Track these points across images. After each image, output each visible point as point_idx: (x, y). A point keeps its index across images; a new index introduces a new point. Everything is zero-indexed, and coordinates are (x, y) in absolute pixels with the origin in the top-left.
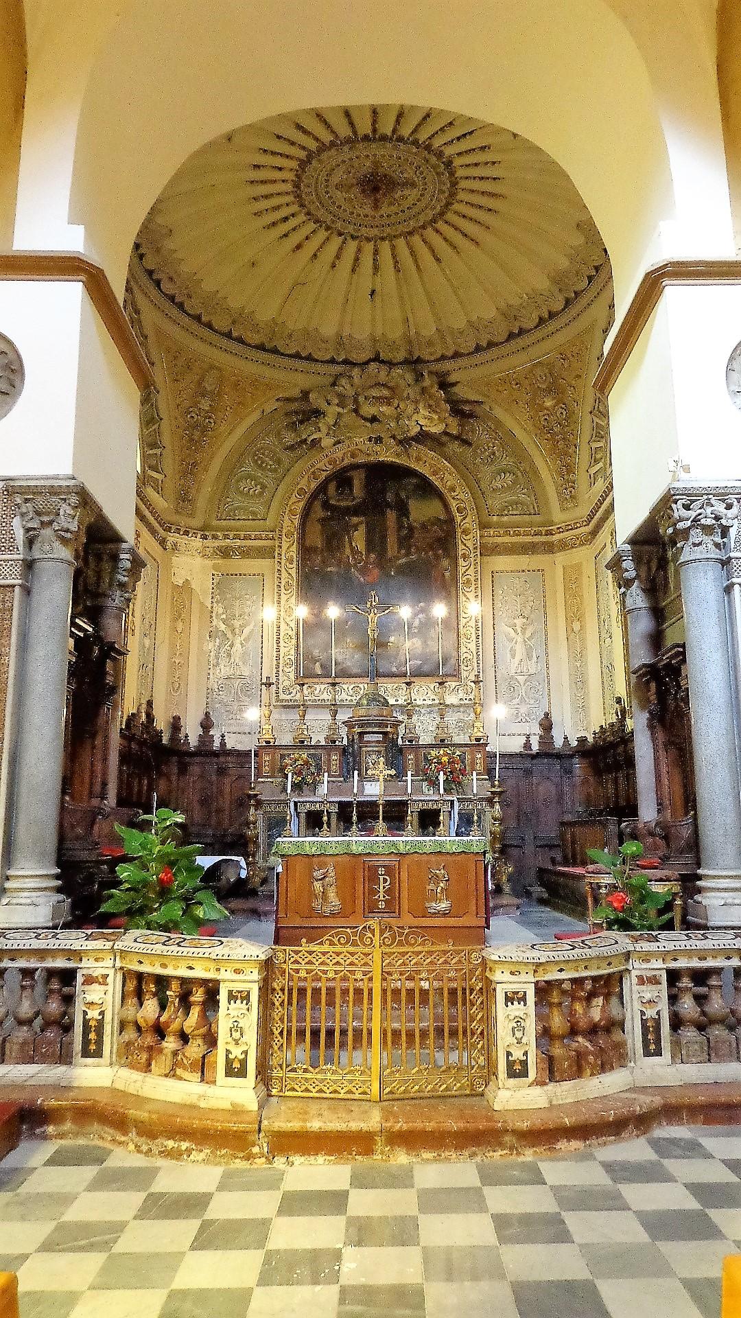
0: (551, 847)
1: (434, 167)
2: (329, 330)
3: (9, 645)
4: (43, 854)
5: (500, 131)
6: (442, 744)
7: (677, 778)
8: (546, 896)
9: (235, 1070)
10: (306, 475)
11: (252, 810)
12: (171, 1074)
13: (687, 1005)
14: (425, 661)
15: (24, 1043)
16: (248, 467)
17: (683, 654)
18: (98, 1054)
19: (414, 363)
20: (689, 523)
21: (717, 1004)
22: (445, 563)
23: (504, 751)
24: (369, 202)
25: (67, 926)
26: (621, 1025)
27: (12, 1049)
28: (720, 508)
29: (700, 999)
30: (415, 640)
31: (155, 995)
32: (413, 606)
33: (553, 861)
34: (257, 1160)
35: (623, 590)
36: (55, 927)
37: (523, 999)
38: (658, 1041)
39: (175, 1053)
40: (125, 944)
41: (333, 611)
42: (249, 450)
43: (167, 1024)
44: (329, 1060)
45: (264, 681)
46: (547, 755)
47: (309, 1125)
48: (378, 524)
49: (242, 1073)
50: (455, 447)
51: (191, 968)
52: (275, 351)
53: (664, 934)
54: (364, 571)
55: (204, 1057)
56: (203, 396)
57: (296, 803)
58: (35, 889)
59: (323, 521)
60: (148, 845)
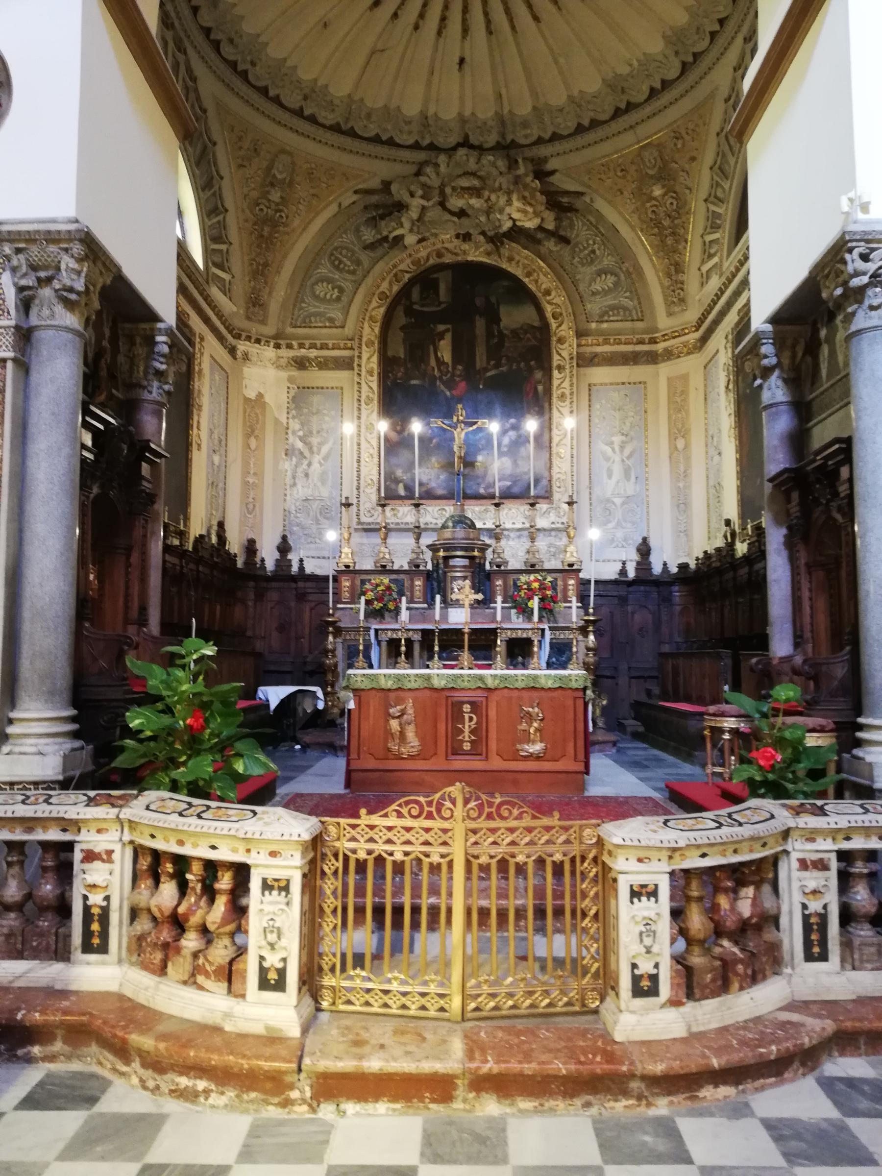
4: (52, 693)
6: (532, 568)
8: (641, 729)
9: (272, 982)
10: (385, 277)
11: (331, 638)
12: (191, 981)
14: (515, 483)
18: (103, 949)
19: (507, 148)
20: (865, 279)
22: (538, 375)
26: (775, 920)
31: (172, 876)
33: (649, 693)
34: (297, 1108)
37: (654, 894)
38: (823, 942)
39: (195, 955)
41: (417, 427)
42: (327, 251)
43: (186, 917)
45: (344, 501)
46: (640, 588)
48: (463, 340)
49: (280, 985)
50: (551, 245)
51: (213, 847)
55: (231, 963)
56: (272, 185)
57: (376, 631)
58: (49, 735)
59: (402, 328)
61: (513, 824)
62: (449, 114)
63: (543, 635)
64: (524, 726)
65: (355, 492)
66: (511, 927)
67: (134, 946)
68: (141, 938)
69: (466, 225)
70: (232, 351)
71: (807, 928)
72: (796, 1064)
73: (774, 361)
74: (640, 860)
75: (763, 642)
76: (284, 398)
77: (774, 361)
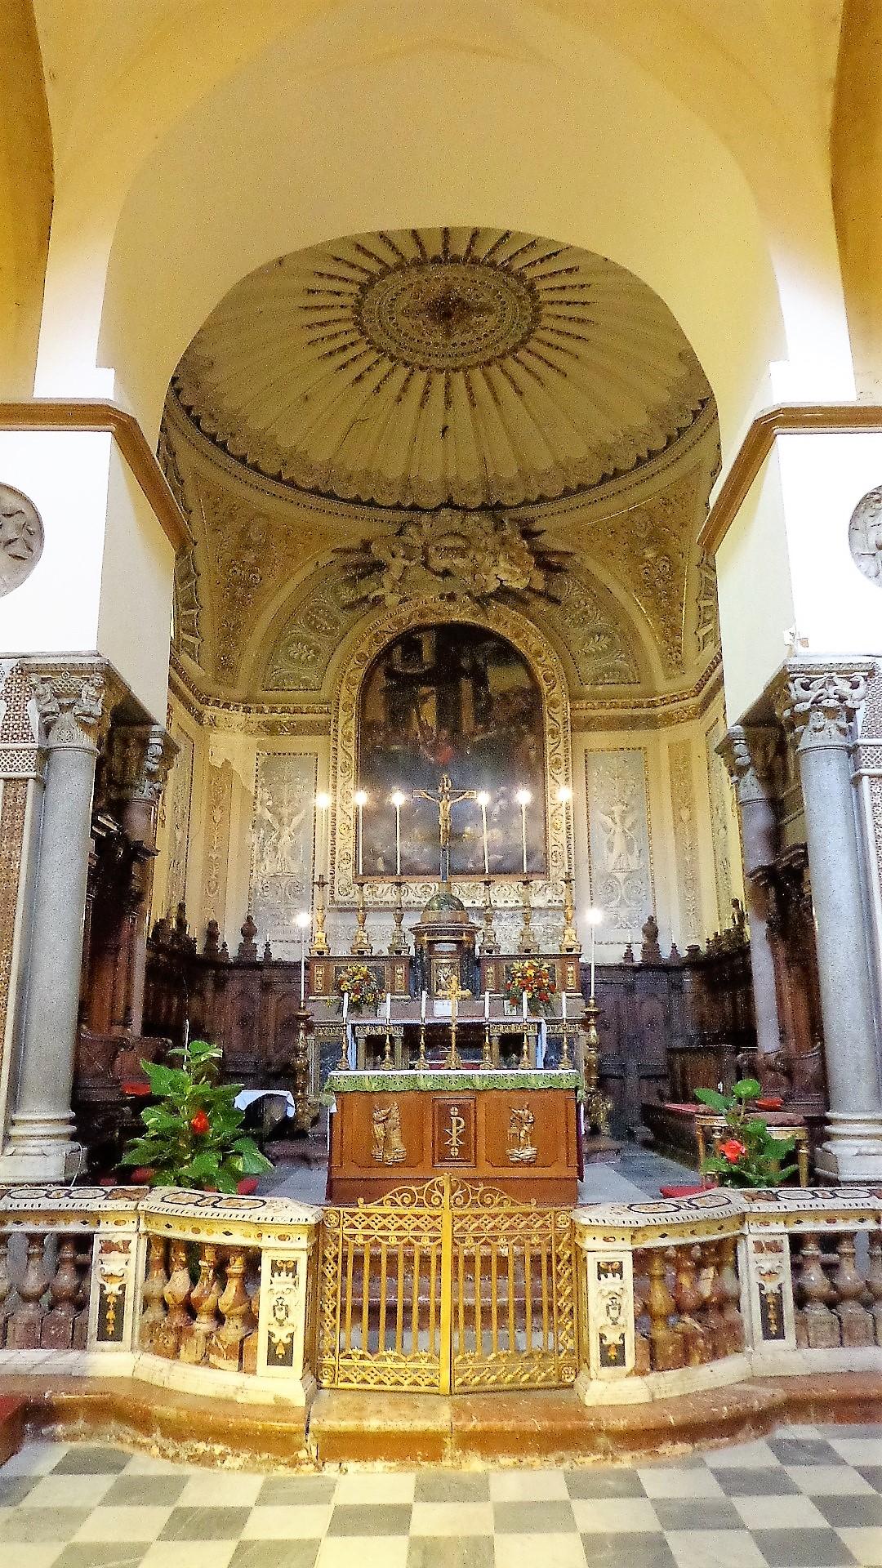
0: (657, 1077)
1: (514, 291)
2: (394, 472)
3: (21, 847)
4: (54, 1095)
5: (587, 253)
6: (527, 954)
7: (801, 999)
8: (651, 1137)
9: (279, 1357)
11: (302, 1034)
12: (204, 1361)
13: (815, 1278)
14: (507, 855)
15: (30, 1325)
16: (300, 630)
17: (805, 855)
18: (117, 1337)
19: (493, 509)
20: (808, 705)
21: (849, 1276)
22: (530, 739)
24: (439, 329)
25: (82, 1181)
26: (737, 1301)
27: (16, 1330)
28: (844, 687)
29: (829, 1269)
30: (495, 831)
31: (185, 1265)
32: (491, 791)
34: (304, 1467)
35: (735, 778)
36: (67, 1183)
37: (619, 1271)
38: (780, 1320)
39: (208, 1337)
40: (151, 1204)
41: (398, 798)
43: (199, 1301)
44: (389, 1344)
46: (652, 968)
47: (365, 1423)
48: (449, 694)
49: (287, 1360)
50: (540, 605)
51: (227, 1233)
52: (331, 495)
53: (784, 1192)
54: (434, 749)
55: (242, 1341)
56: (247, 547)
57: (353, 1026)
59: (386, 690)
60: (180, 1082)
61: (495, 1210)
62: (432, 476)
63: (539, 1030)
64: (514, 1130)
65: (329, 868)
66: (495, 1326)
67: (147, 1333)
68: (153, 1325)
69: (450, 585)
70: (199, 717)
71: (765, 1307)
72: (748, 1426)
73: (747, 760)
74: (605, 1239)
76: (252, 765)
77: (747, 760)
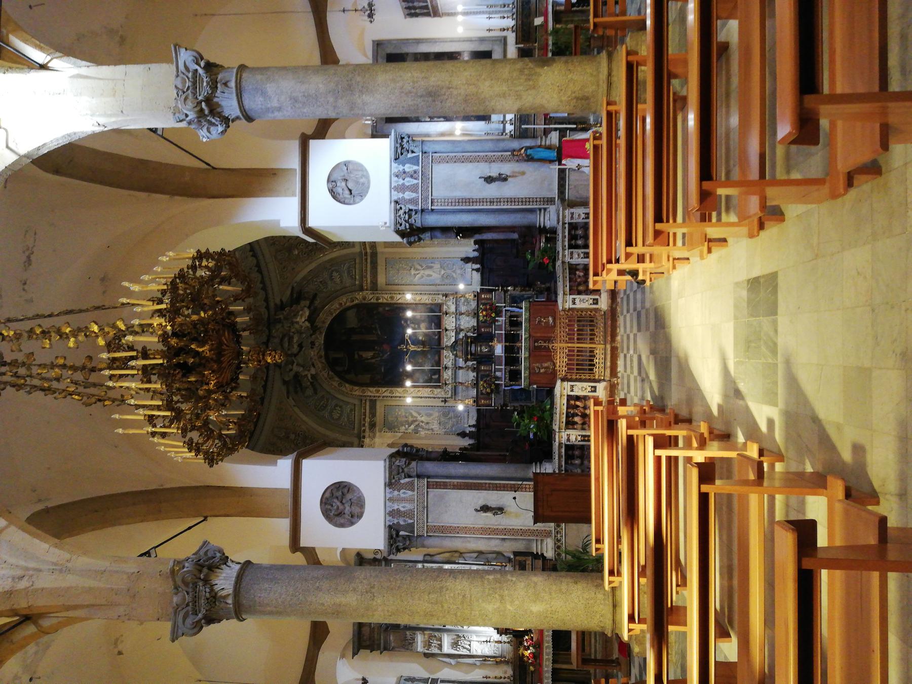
6: (476, 315)
9: (594, 389)
19: (271, 323)
22: (381, 309)
23: (479, 283)
28: (401, 212)
37: (574, 299)
49: (595, 387)
50: (317, 303)
56: (288, 437)
75: (514, 240)
76: (389, 434)
